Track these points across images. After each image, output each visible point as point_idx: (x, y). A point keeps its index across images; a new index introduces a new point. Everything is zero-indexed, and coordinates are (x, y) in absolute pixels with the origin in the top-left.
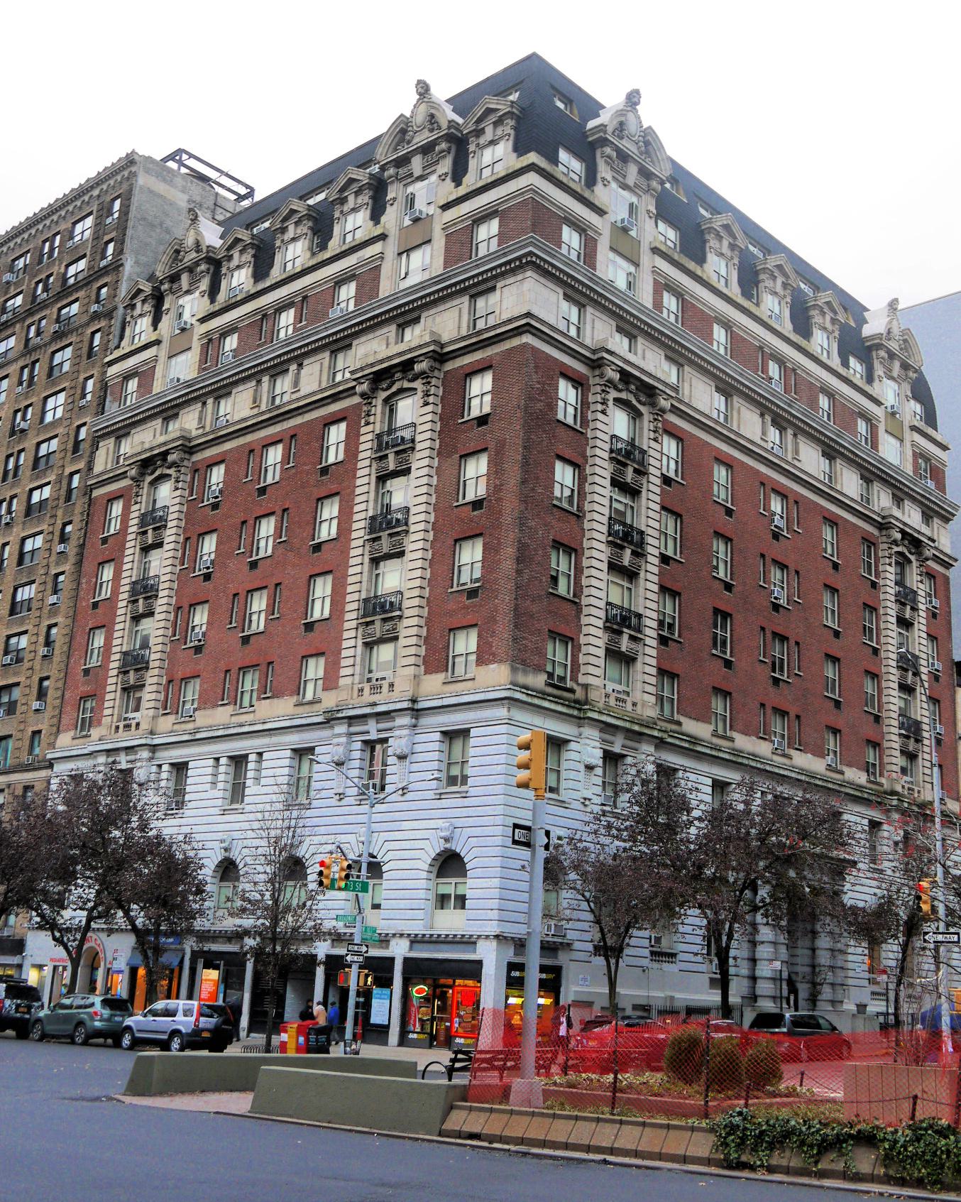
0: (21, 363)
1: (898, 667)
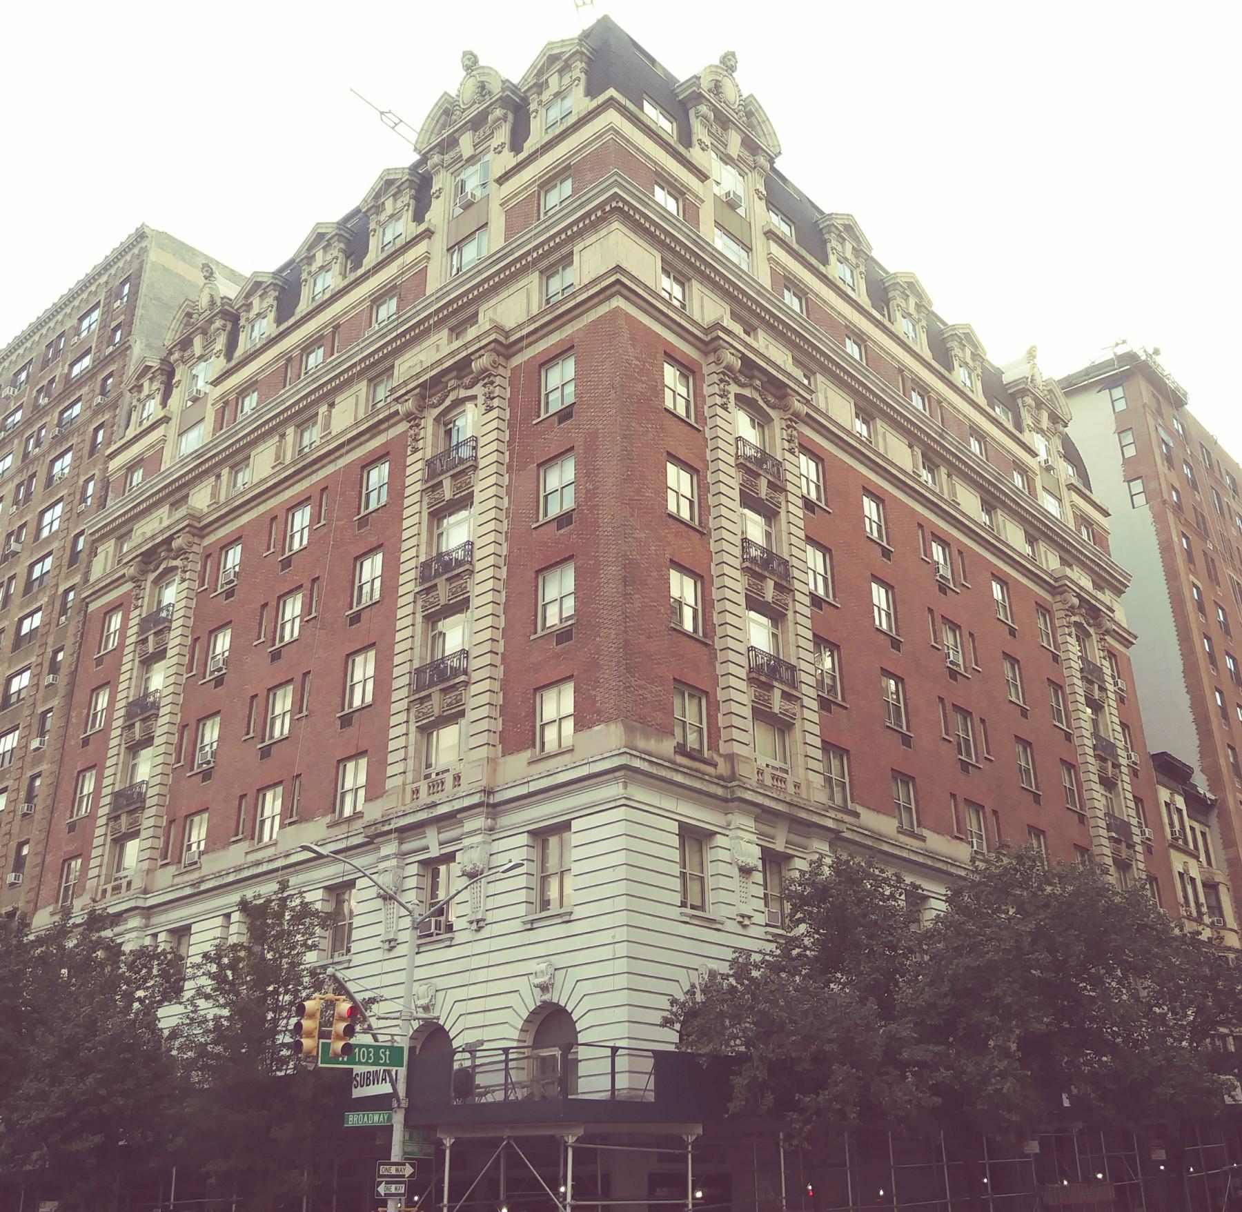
0: (17, 481)
1: (1095, 756)
